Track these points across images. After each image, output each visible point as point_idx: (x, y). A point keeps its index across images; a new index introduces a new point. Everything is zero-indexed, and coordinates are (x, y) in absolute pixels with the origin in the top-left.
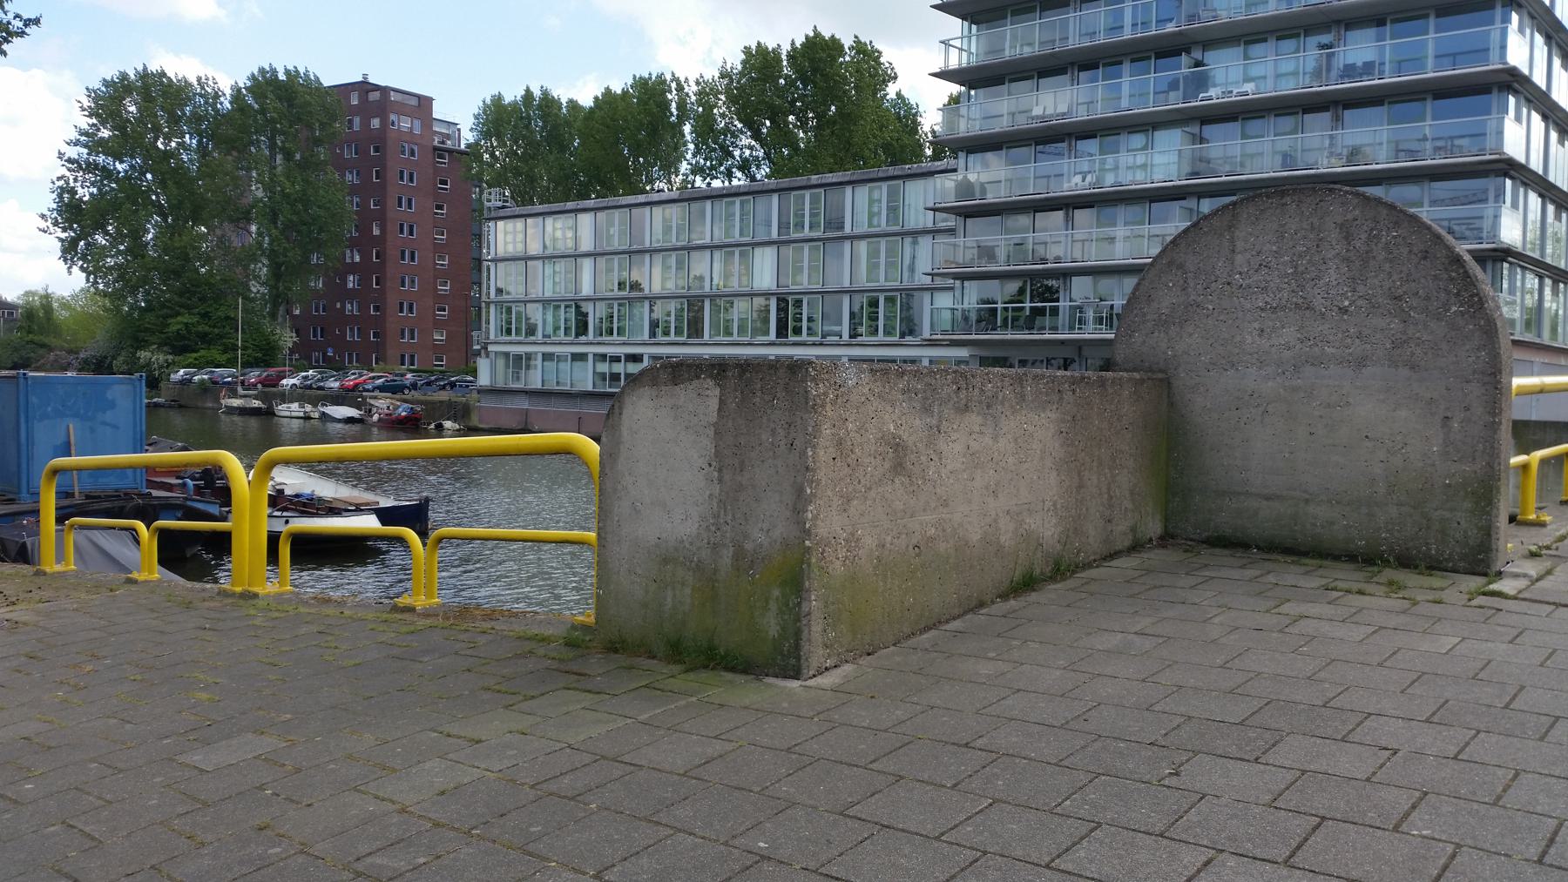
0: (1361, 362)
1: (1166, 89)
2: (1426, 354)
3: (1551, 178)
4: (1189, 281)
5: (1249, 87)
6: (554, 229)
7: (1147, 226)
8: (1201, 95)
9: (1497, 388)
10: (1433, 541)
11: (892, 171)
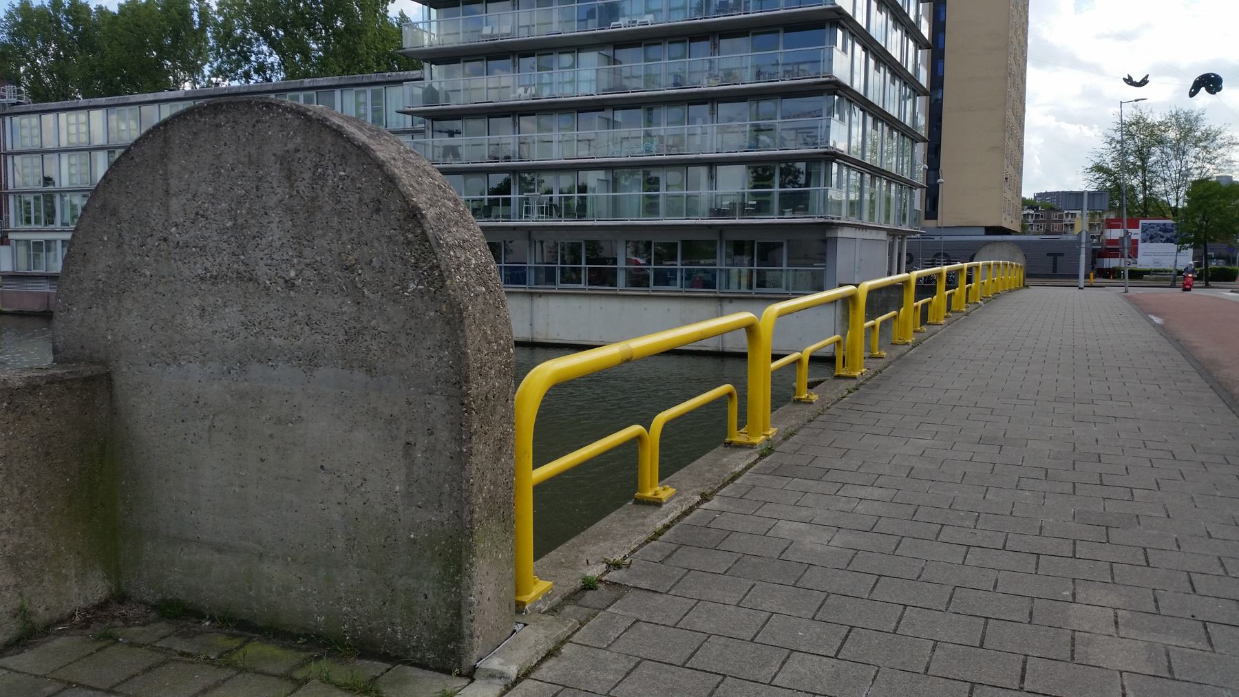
0: (311, 360)
1: (586, 18)
2: (383, 350)
3: (870, 98)
4: (124, 233)
5: (649, 18)
6: (68, 124)
7: (686, 126)
8: (613, 23)
9: (463, 404)
10: (399, 621)
11: (374, 77)
